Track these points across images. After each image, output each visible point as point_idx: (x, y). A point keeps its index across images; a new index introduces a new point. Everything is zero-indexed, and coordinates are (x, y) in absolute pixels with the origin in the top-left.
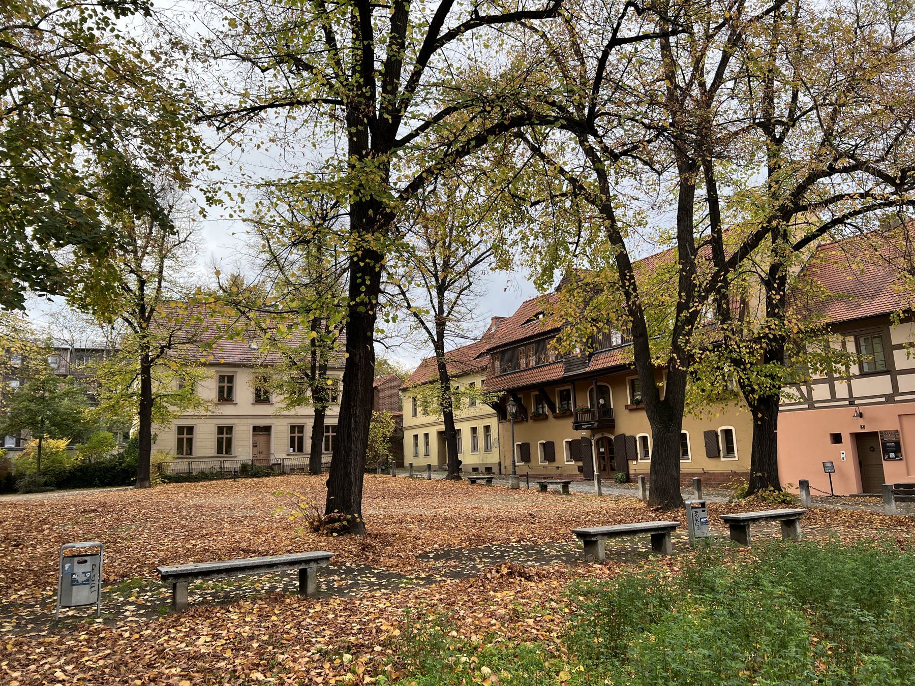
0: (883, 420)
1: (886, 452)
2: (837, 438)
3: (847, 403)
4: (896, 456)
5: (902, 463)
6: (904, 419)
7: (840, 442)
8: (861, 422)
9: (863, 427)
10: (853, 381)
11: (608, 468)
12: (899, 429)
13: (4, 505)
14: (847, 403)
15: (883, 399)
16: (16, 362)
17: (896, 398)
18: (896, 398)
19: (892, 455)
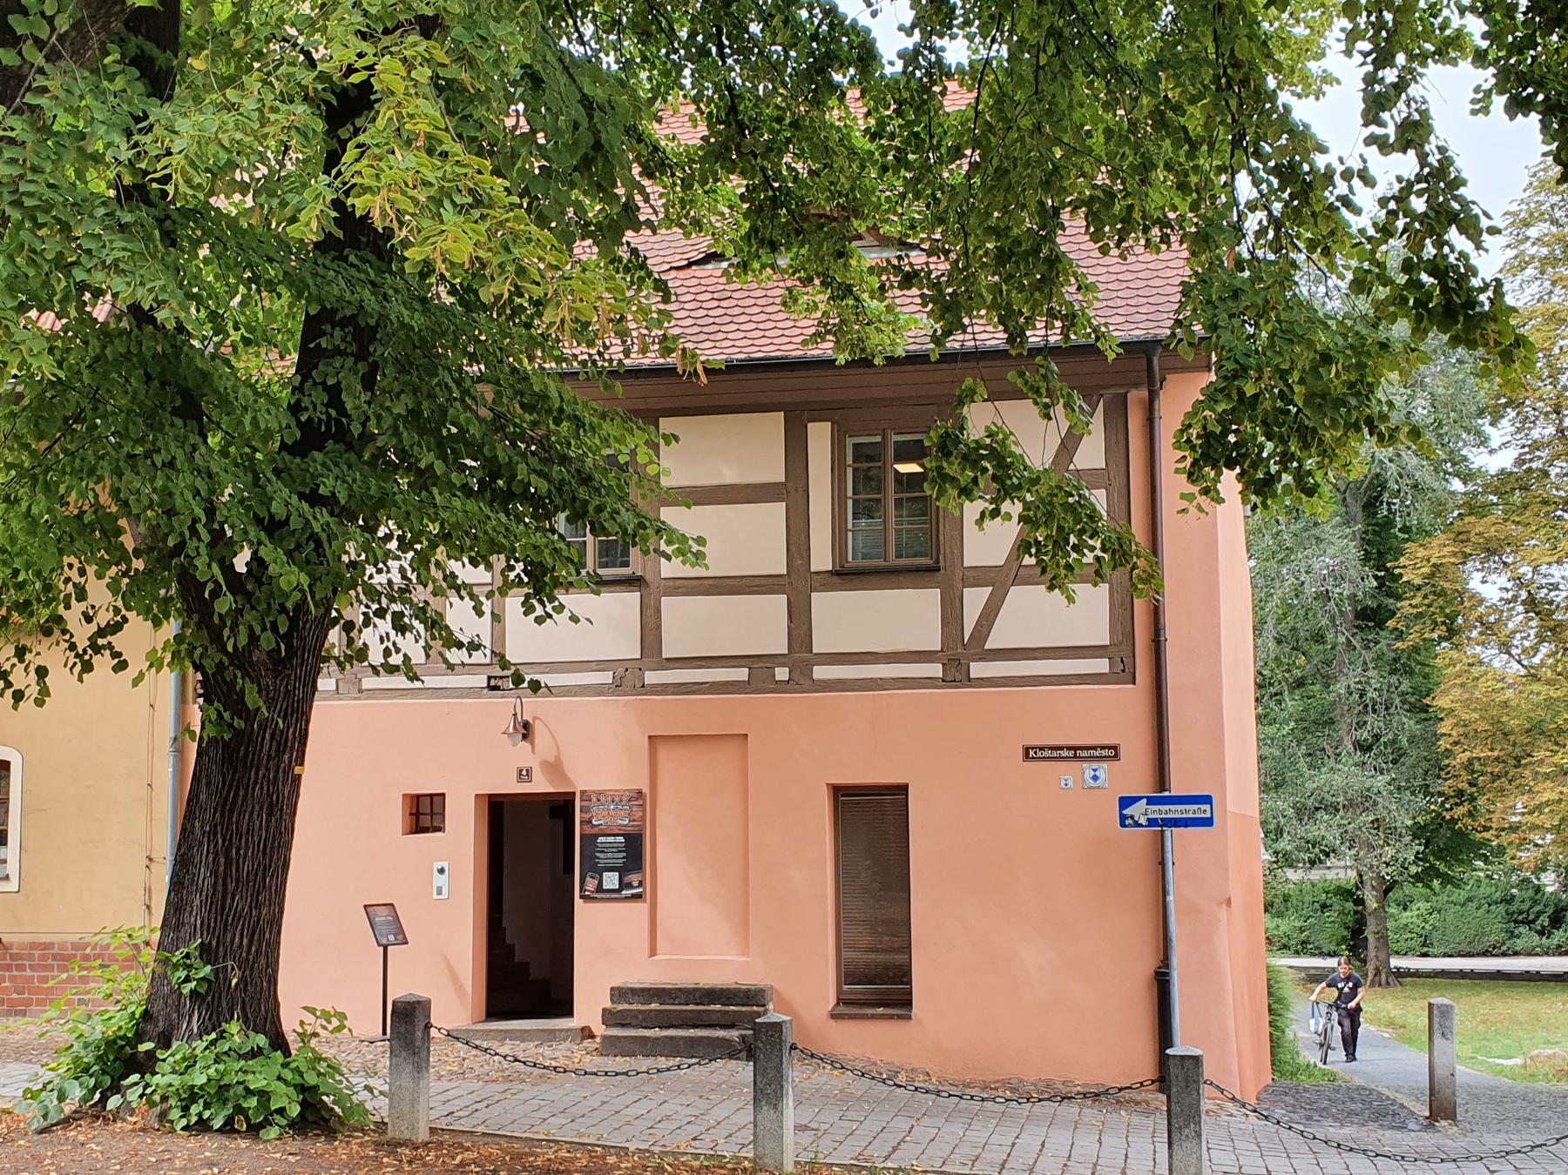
0: (593, 754)
1: (593, 868)
2: (424, 814)
3: (935, 670)
4: (623, 885)
5: (641, 908)
6: (664, 752)
7: (417, 828)
8: (523, 755)
9: (524, 775)
10: (777, 564)
11: (425, 807)
12: (646, 790)
13: (1561, 951)
14: (935, 670)
15: (742, 674)
16: (1531, 1124)
17: (651, 677)
18: (651, 677)
19: (611, 880)
